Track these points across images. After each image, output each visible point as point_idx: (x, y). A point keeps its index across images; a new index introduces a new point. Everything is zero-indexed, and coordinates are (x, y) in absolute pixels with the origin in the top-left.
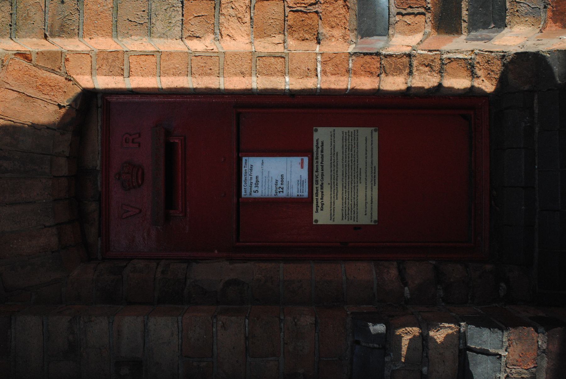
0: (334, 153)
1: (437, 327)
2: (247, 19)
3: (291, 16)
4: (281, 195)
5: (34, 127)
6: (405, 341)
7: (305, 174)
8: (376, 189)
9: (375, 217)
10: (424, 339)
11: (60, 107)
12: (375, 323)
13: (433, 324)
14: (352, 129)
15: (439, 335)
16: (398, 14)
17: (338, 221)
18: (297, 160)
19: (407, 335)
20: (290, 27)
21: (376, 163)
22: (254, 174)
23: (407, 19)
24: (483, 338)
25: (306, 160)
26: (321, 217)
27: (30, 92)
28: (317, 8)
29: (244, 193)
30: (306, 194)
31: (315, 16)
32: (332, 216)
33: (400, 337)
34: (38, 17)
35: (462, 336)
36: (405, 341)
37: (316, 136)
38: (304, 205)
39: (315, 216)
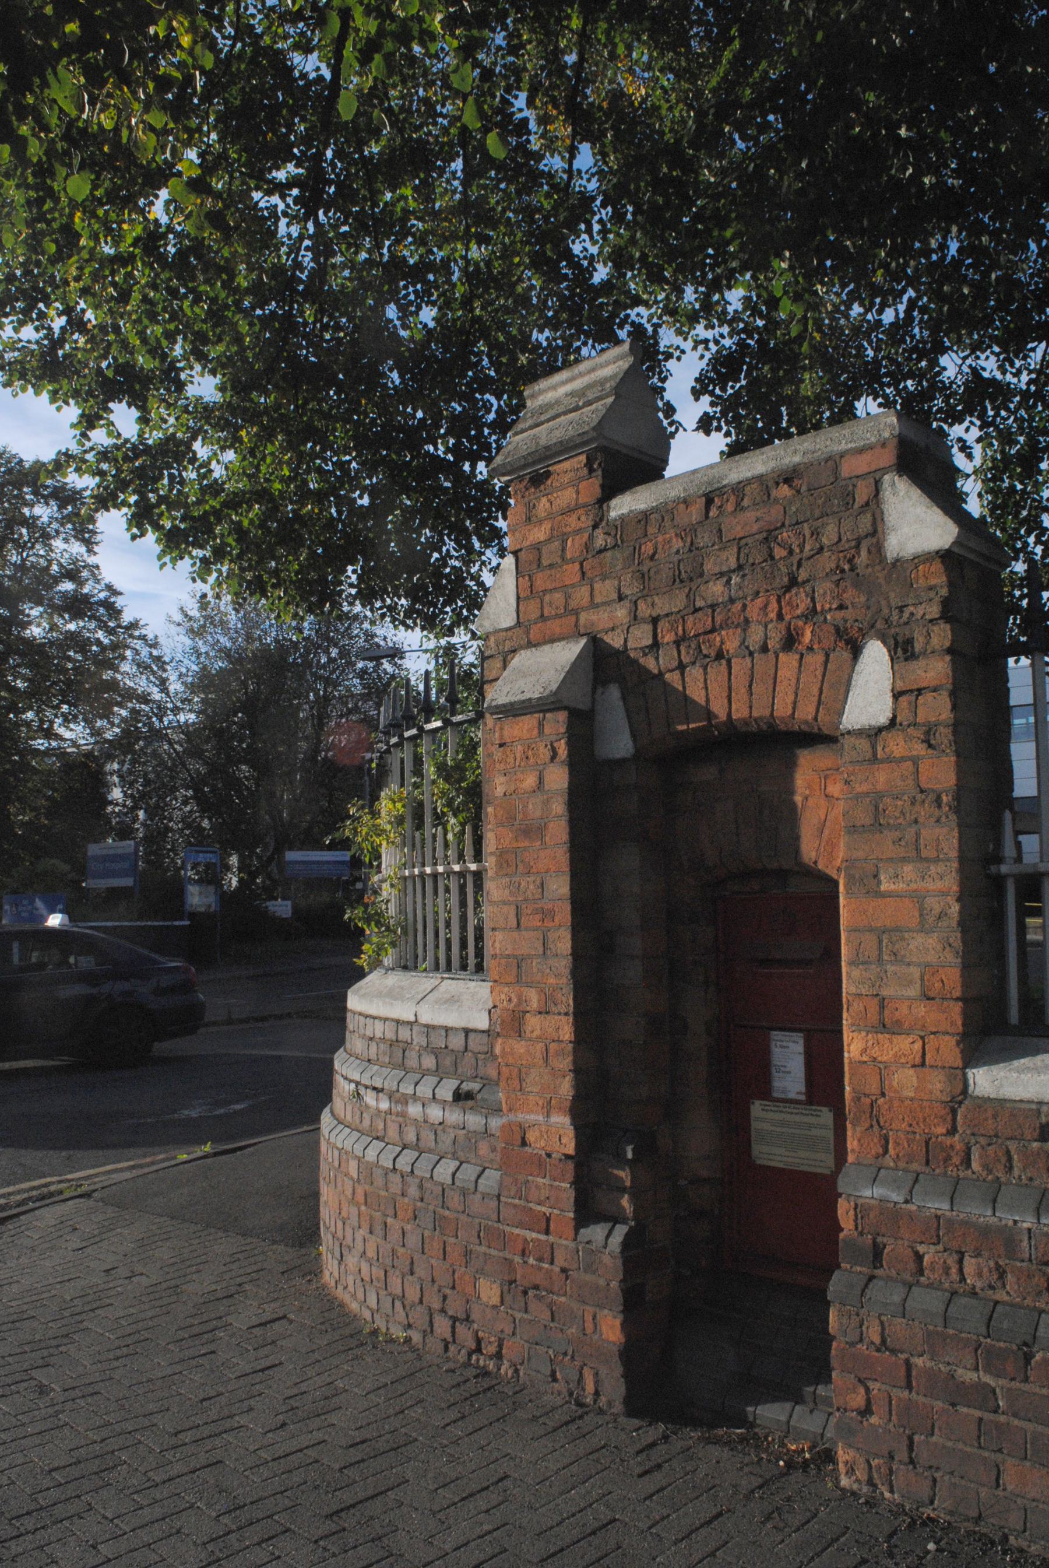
0: (810, 1126)
1: (631, 1200)
2: (865, 1058)
3: (868, 1101)
4: (773, 1070)
5: (797, 838)
6: (621, 1174)
7: (792, 1095)
8: (781, 1165)
9: (759, 1162)
10: (623, 1190)
11: (815, 862)
12: (633, 1150)
13: (635, 1198)
14: (832, 1146)
15: (625, 1202)
16: (856, 1205)
17: (755, 1125)
18: (803, 1090)
19: (624, 1175)
20: (859, 1099)
21: (801, 1168)
22: (791, 1044)
23: (852, 1213)
24: (620, 1232)
25: (803, 1098)
26: (757, 1108)
27: (826, 832)
28: (876, 1128)
29: (776, 1035)
30: (775, 1095)
31: (867, 1125)
32: (757, 1119)
33: (624, 1170)
34: (860, 854)
35: (624, 1221)
36: (621, 1174)
37: (825, 1109)
38: (765, 1092)
39: (757, 1103)
